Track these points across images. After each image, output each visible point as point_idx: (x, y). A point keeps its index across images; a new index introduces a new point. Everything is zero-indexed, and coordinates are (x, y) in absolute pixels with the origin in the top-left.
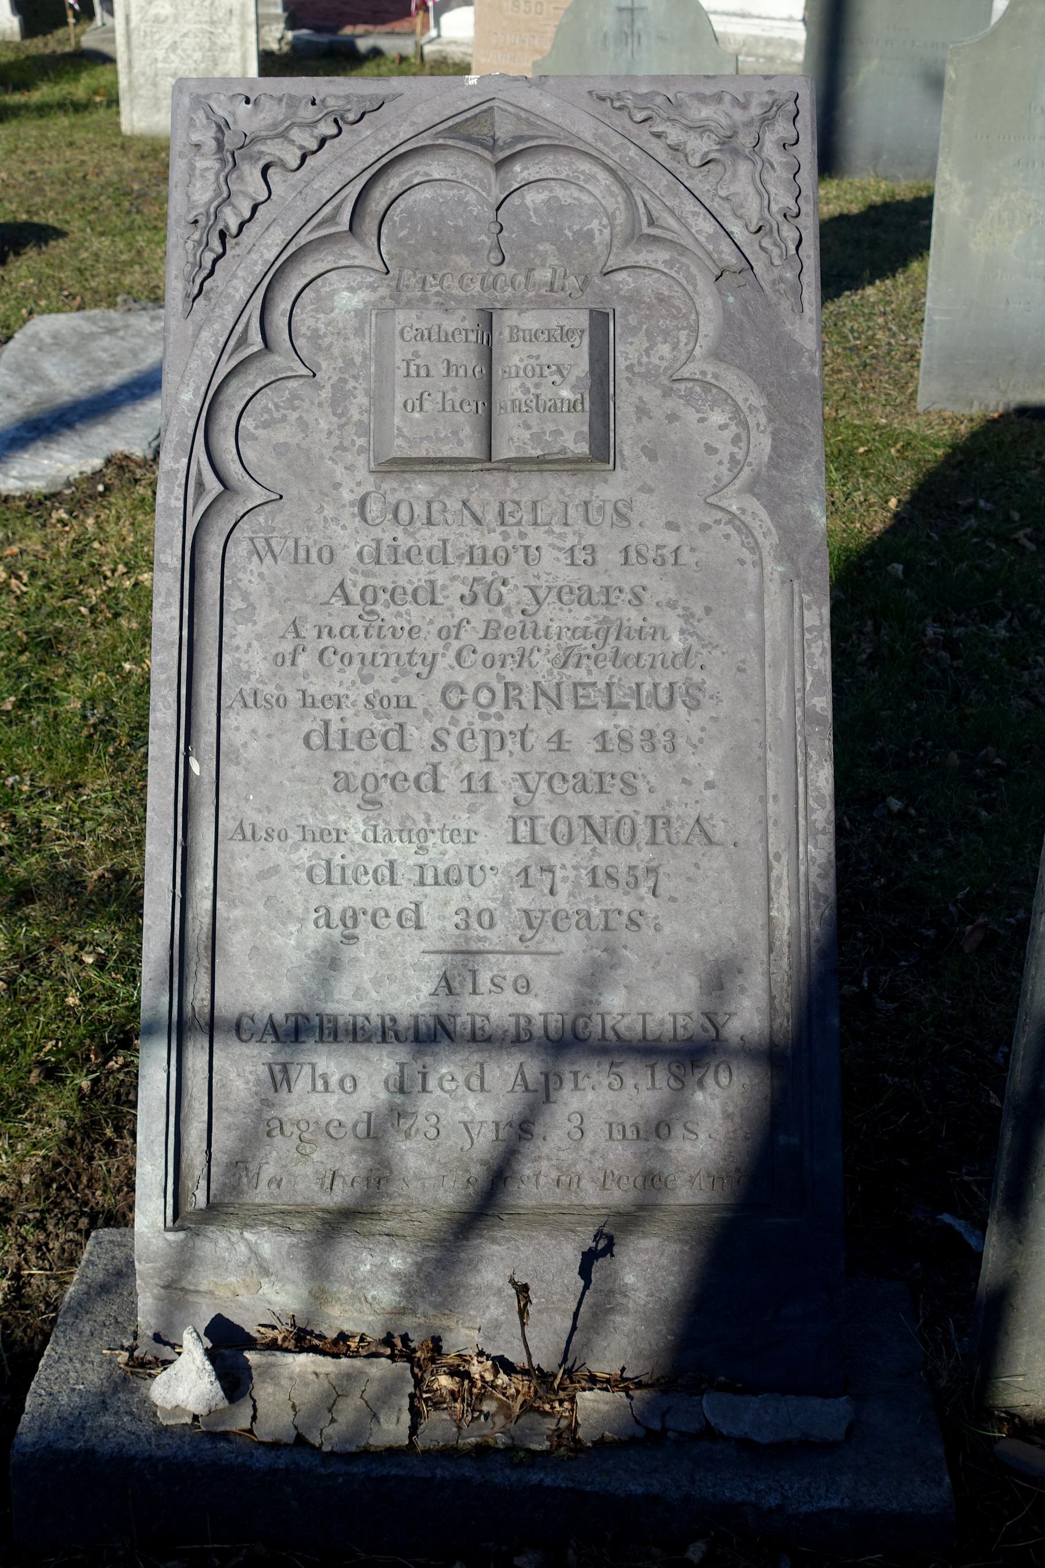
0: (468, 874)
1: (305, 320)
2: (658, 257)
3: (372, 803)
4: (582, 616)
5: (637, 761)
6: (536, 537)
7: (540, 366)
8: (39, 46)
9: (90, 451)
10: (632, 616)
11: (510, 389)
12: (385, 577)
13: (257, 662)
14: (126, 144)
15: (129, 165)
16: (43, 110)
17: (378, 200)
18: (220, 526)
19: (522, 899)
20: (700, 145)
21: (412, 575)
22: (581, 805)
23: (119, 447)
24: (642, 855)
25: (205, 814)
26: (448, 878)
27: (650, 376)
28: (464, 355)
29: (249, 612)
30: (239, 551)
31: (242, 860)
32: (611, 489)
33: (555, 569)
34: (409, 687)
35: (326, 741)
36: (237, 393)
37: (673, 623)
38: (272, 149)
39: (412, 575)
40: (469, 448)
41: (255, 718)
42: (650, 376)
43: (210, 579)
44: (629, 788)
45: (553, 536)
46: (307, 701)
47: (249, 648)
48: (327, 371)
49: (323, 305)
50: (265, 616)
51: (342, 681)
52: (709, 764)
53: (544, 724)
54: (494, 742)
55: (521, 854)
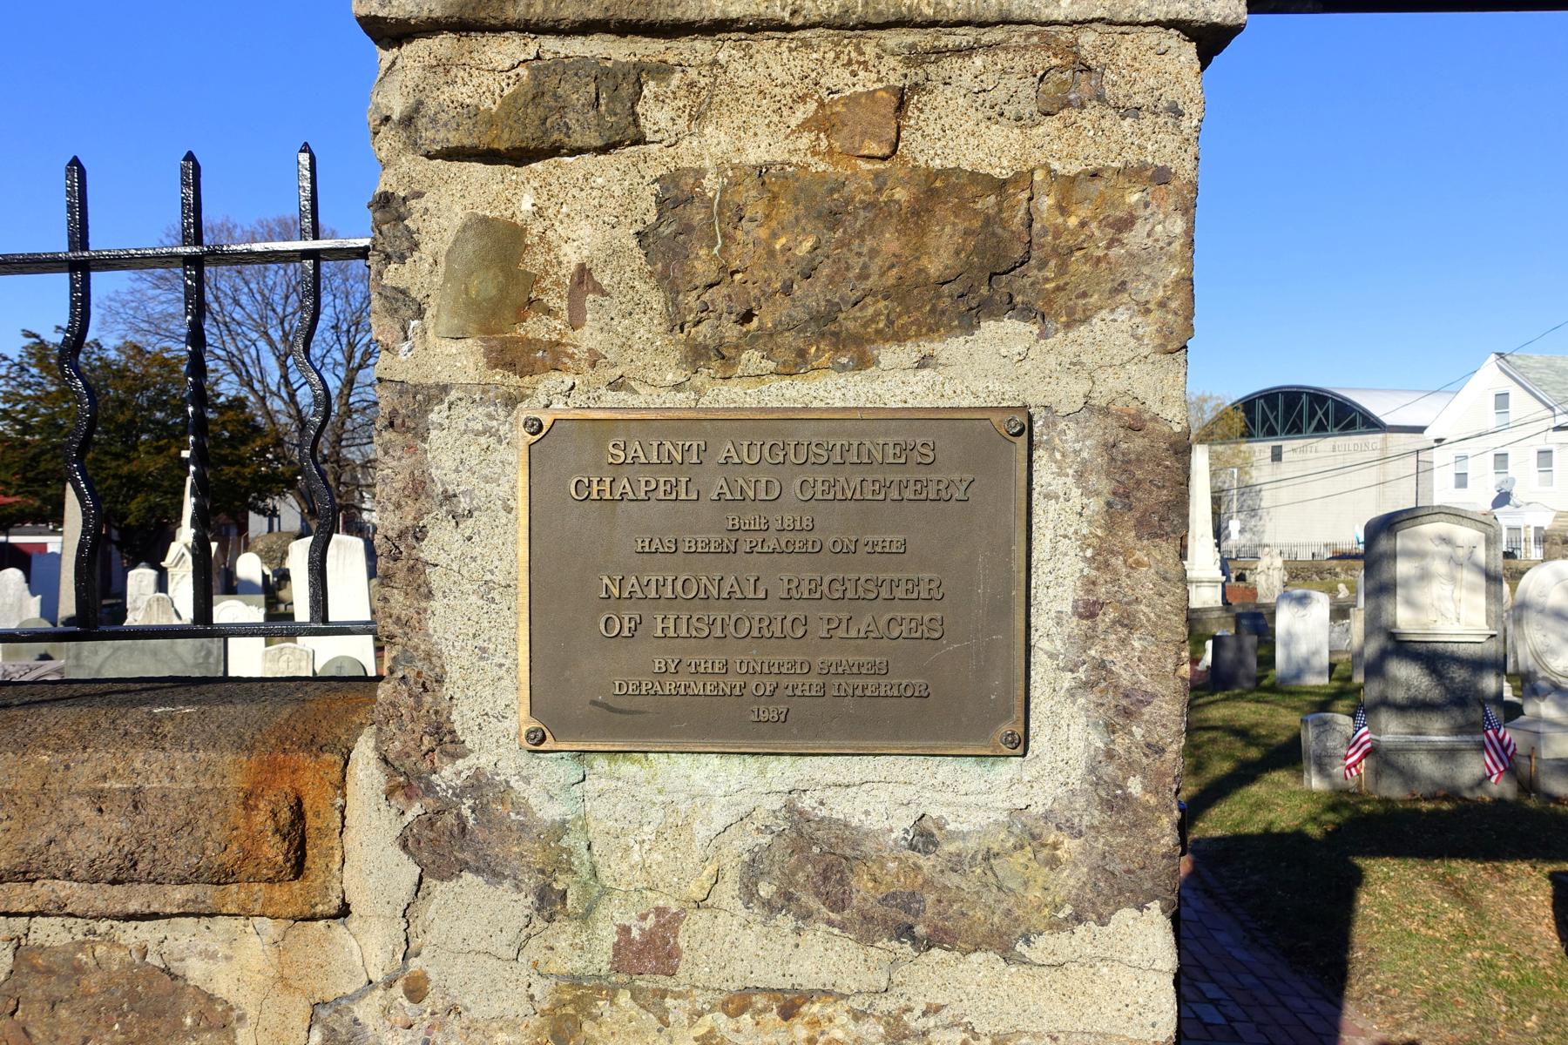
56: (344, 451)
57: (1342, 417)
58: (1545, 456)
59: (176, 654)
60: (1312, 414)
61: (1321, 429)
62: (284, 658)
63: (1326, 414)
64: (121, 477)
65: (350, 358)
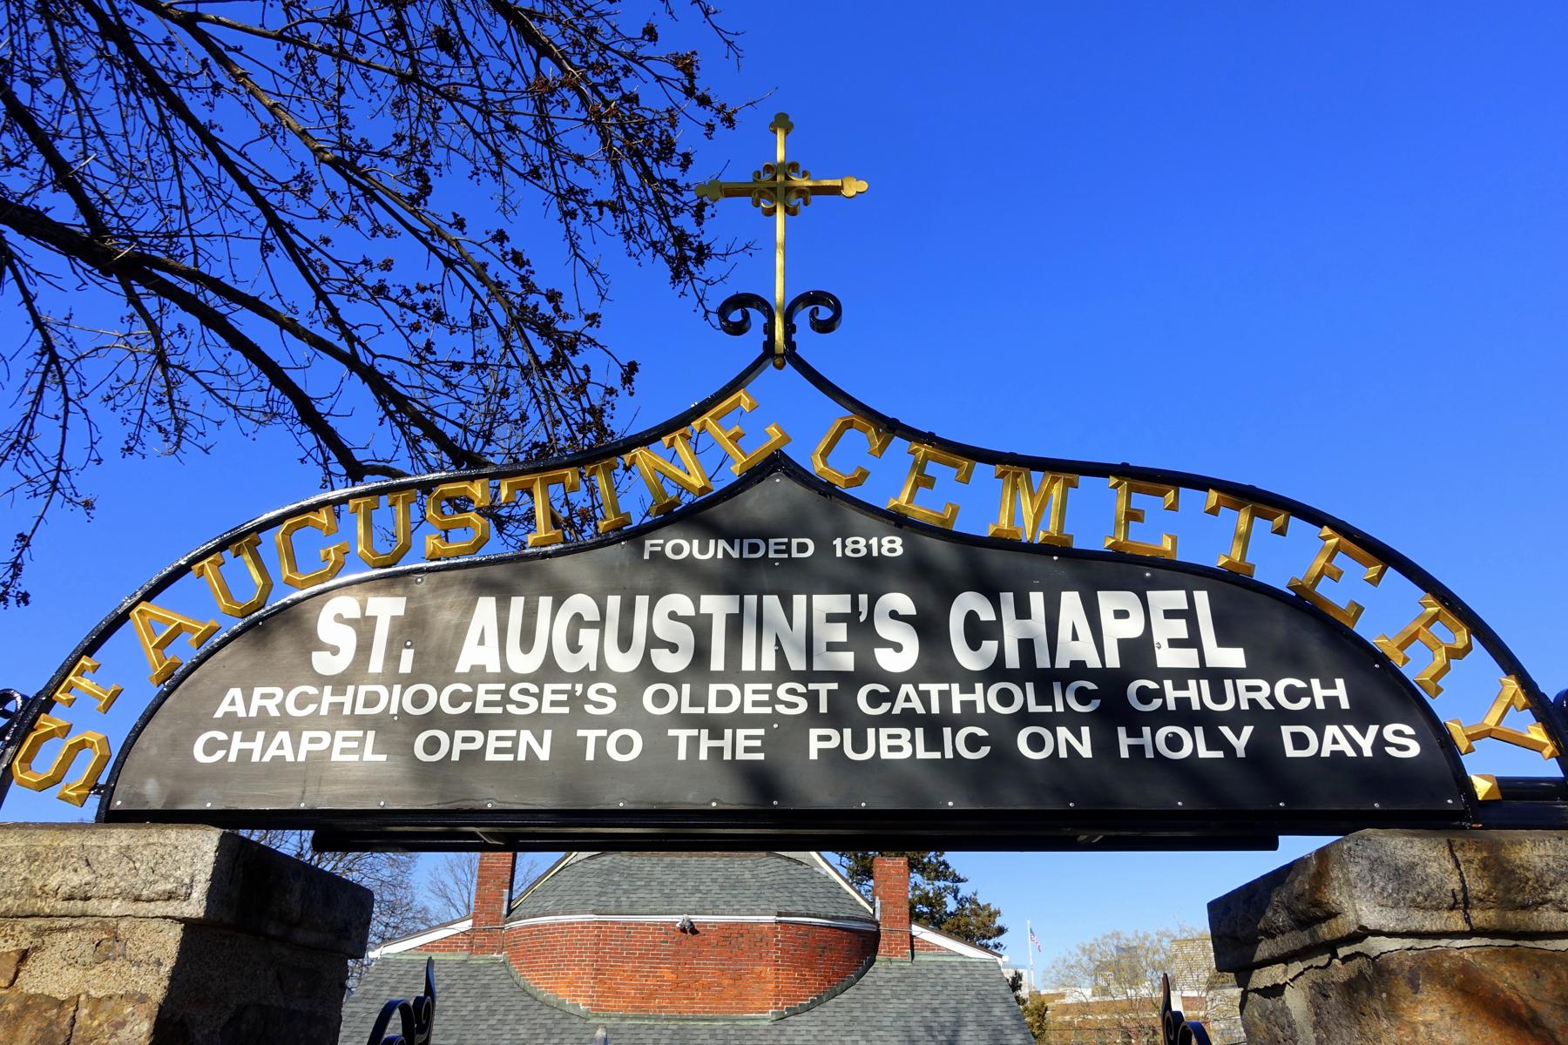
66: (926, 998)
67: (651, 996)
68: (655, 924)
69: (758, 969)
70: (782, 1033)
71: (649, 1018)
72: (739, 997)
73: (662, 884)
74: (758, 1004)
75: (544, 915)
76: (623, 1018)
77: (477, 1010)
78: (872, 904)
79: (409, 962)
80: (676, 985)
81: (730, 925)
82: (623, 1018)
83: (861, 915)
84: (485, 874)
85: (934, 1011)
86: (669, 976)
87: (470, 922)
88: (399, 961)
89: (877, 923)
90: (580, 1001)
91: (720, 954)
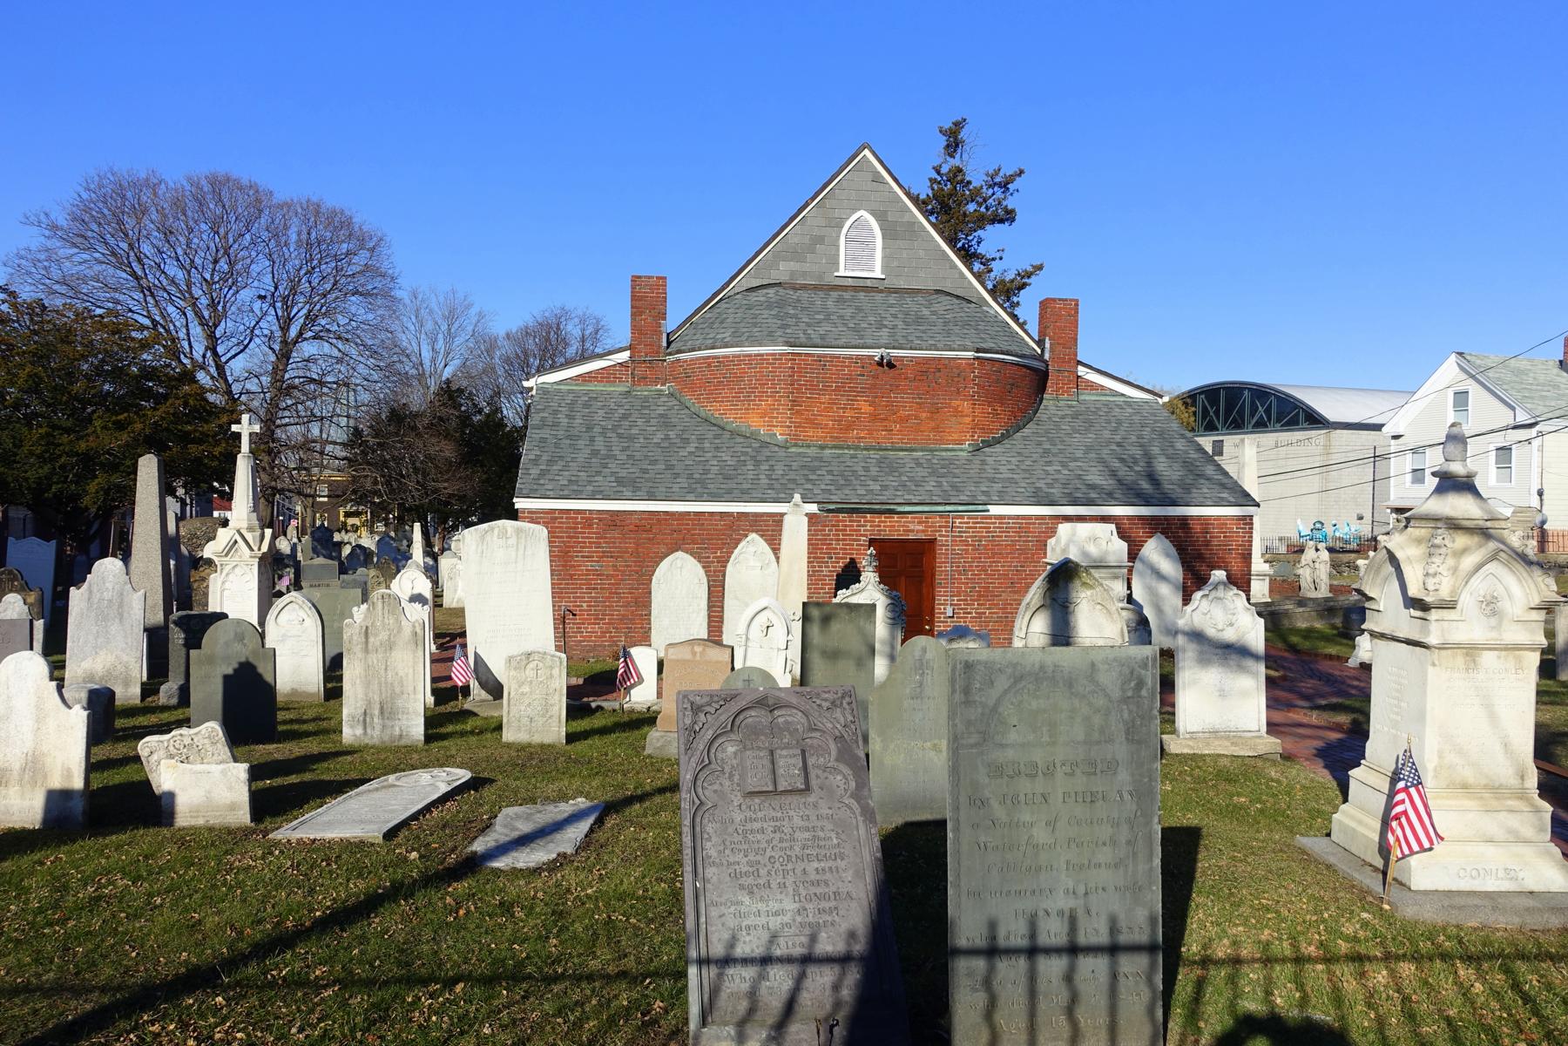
0: (783, 912)
1: (720, 755)
2: (817, 734)
3: (751, 893)
4: (807, 835)
5: (828, 876)
6: (792, 813)
7: (789, 766)
8: (442, 709)
9: (550, 852)
10: (821, 834)
11: (781, 771)
12: (749, 826)
13: (713, 853)
14: (509, 745)
15: (514, 754)
16: (463, 734)
17: (738, 722)
18: (700, 814)
19: (799, 919)
20: (825, 704)
21: (756, 825)
22: (813, 890)
23: (562, 850)
24: (833, 904)
25: (702, 898)
26: (776, 914)
27: (818, 767)
28: (766, 762)
29: (709, 839)
30: (705, 821)
31: (714, 912)
32: (811, 799)
33: (797, 821)
34: (759, 858)
35: (736, 876)
36: (702, 776)
37: (833, 835)
38: (708, 709)
39: (756, 825)
40: (771, 788)
41: (714, 869)
42: (818, 767)
43: (698, 829)
44: (826, 884)
45: (795, 814)
46: (729, 864)
47: (710, 849)
48: (727, 769)
49: (724, 751)
50: (714, 839)
51: (739, 857)
52: (849, 876)
53: (800, 866)
54: (785, 873)
55: (797, 905)
56: (278, 431)
57: (1277, 411)
58: (1504, 452)
59: (1097, 684)
60: (1254, 410)
61: (1261, 426)
62: (531, 665)
63: (1268, 411)
64: (77, 454)
65: (285, 329)
66: (1107, 434)
67: (849, 428)
68: (850, 358)
69: (955, 403)
70: (983, 462)
71: (849, 448)
72: (936, 429)
73: (842, 317)
74: (955, 436)
75: (726, 346)
76: (822, 448)
77: (667, 438)
78: (1040, 343)
79: (570, 391)
80: (874, 417)
81: (928, 360)
82: (822, 448)
83: (1027, 352)
84: (638, 304)
85: (1119, 444)
86: (866, 408)
87: (627, 353)
88: (559, 391)
89: (1046, 362)
90: (777, 431)
91: (917, 388)
